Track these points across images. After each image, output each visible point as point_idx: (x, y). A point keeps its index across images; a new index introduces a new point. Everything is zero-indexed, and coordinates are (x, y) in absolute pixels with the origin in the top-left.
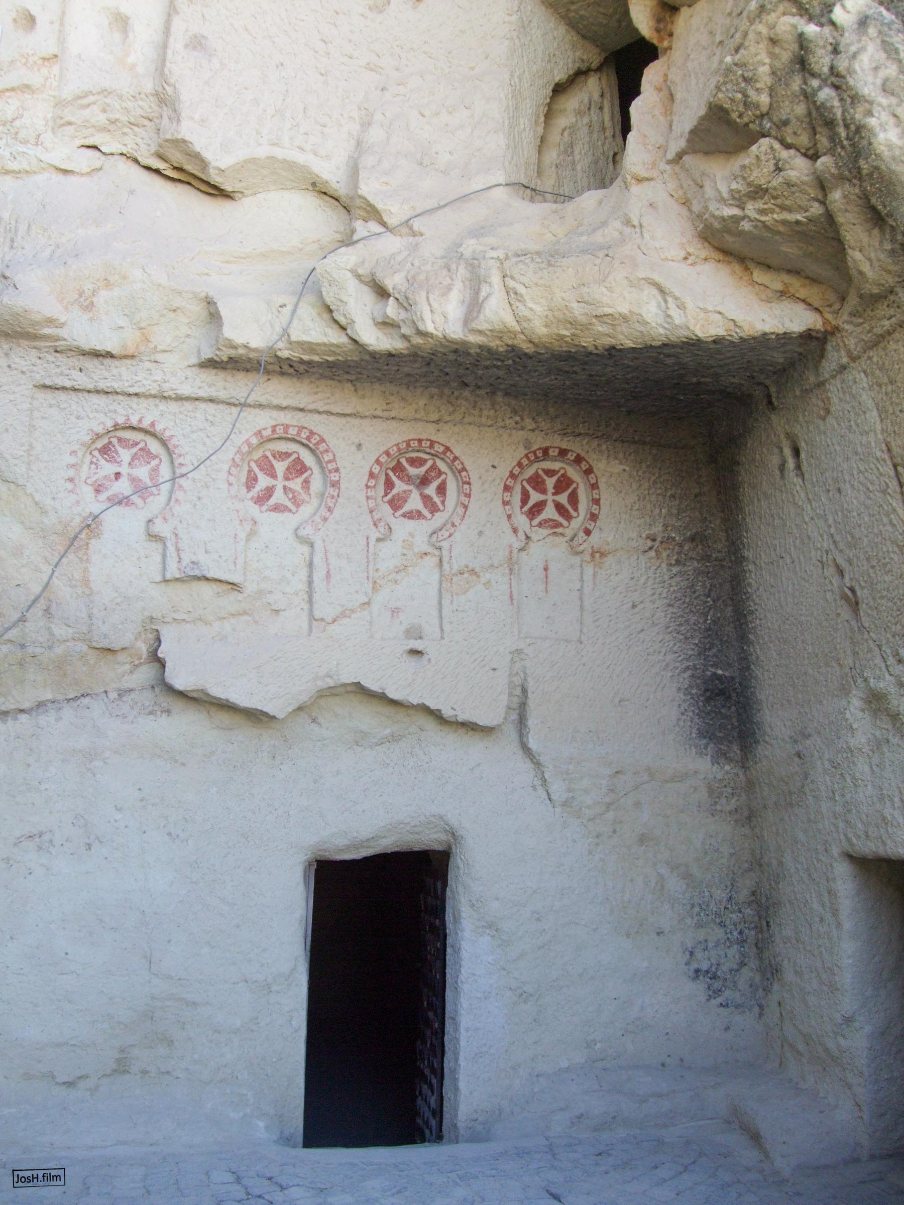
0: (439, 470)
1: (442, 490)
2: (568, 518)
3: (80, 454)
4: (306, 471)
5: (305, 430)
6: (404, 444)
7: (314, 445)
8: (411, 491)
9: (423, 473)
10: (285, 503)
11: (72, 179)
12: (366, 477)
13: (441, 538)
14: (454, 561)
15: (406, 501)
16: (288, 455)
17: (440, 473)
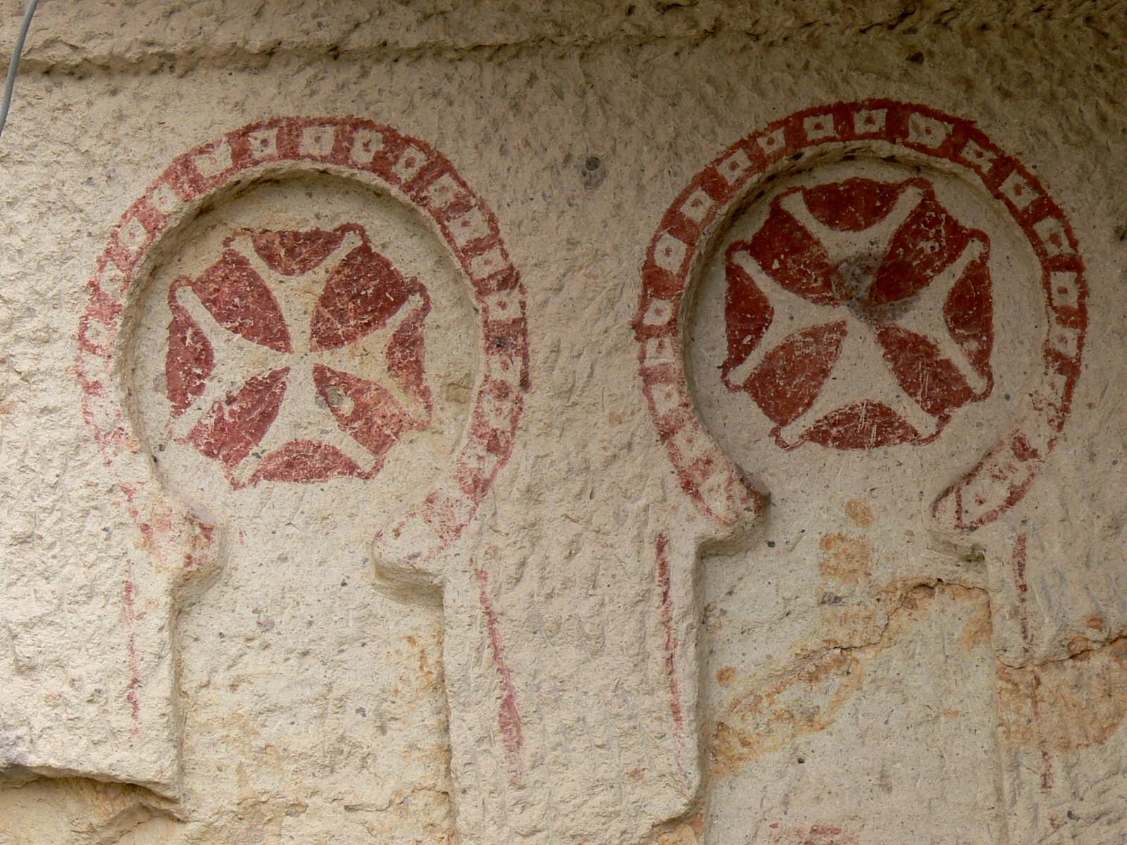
0: (953, 226)
4: (400, 300)
5: (362, 135)
6: (779, 136)
7: (408, 188)
8: (840, 328)
9: (883, 246)
10: (328, 440)
12: (632, 295)
13: (977, 512)
14: (1037, 602)
15: (825, 373)
16: (322, 242)
17: (958, 237)
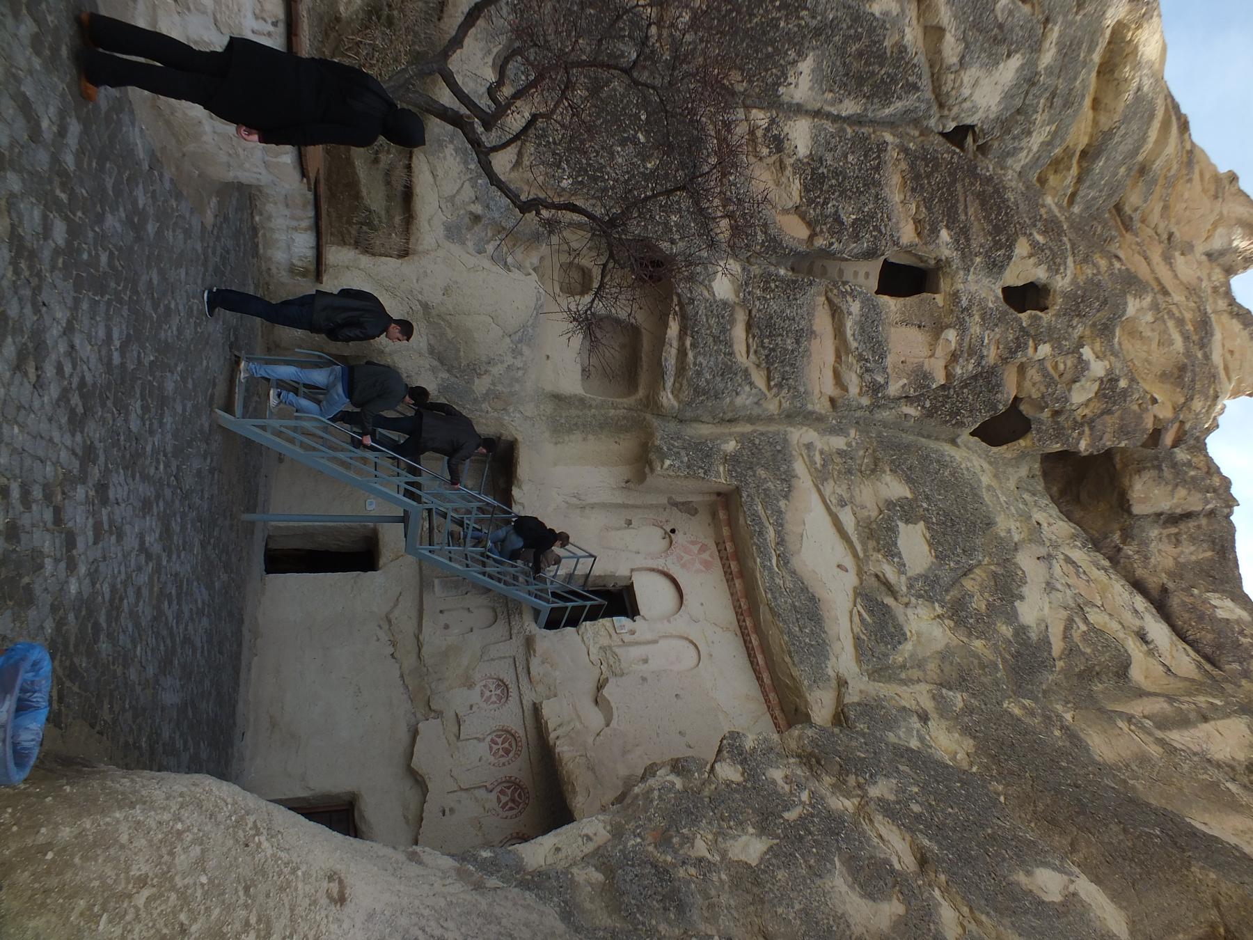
1: (511, 809)
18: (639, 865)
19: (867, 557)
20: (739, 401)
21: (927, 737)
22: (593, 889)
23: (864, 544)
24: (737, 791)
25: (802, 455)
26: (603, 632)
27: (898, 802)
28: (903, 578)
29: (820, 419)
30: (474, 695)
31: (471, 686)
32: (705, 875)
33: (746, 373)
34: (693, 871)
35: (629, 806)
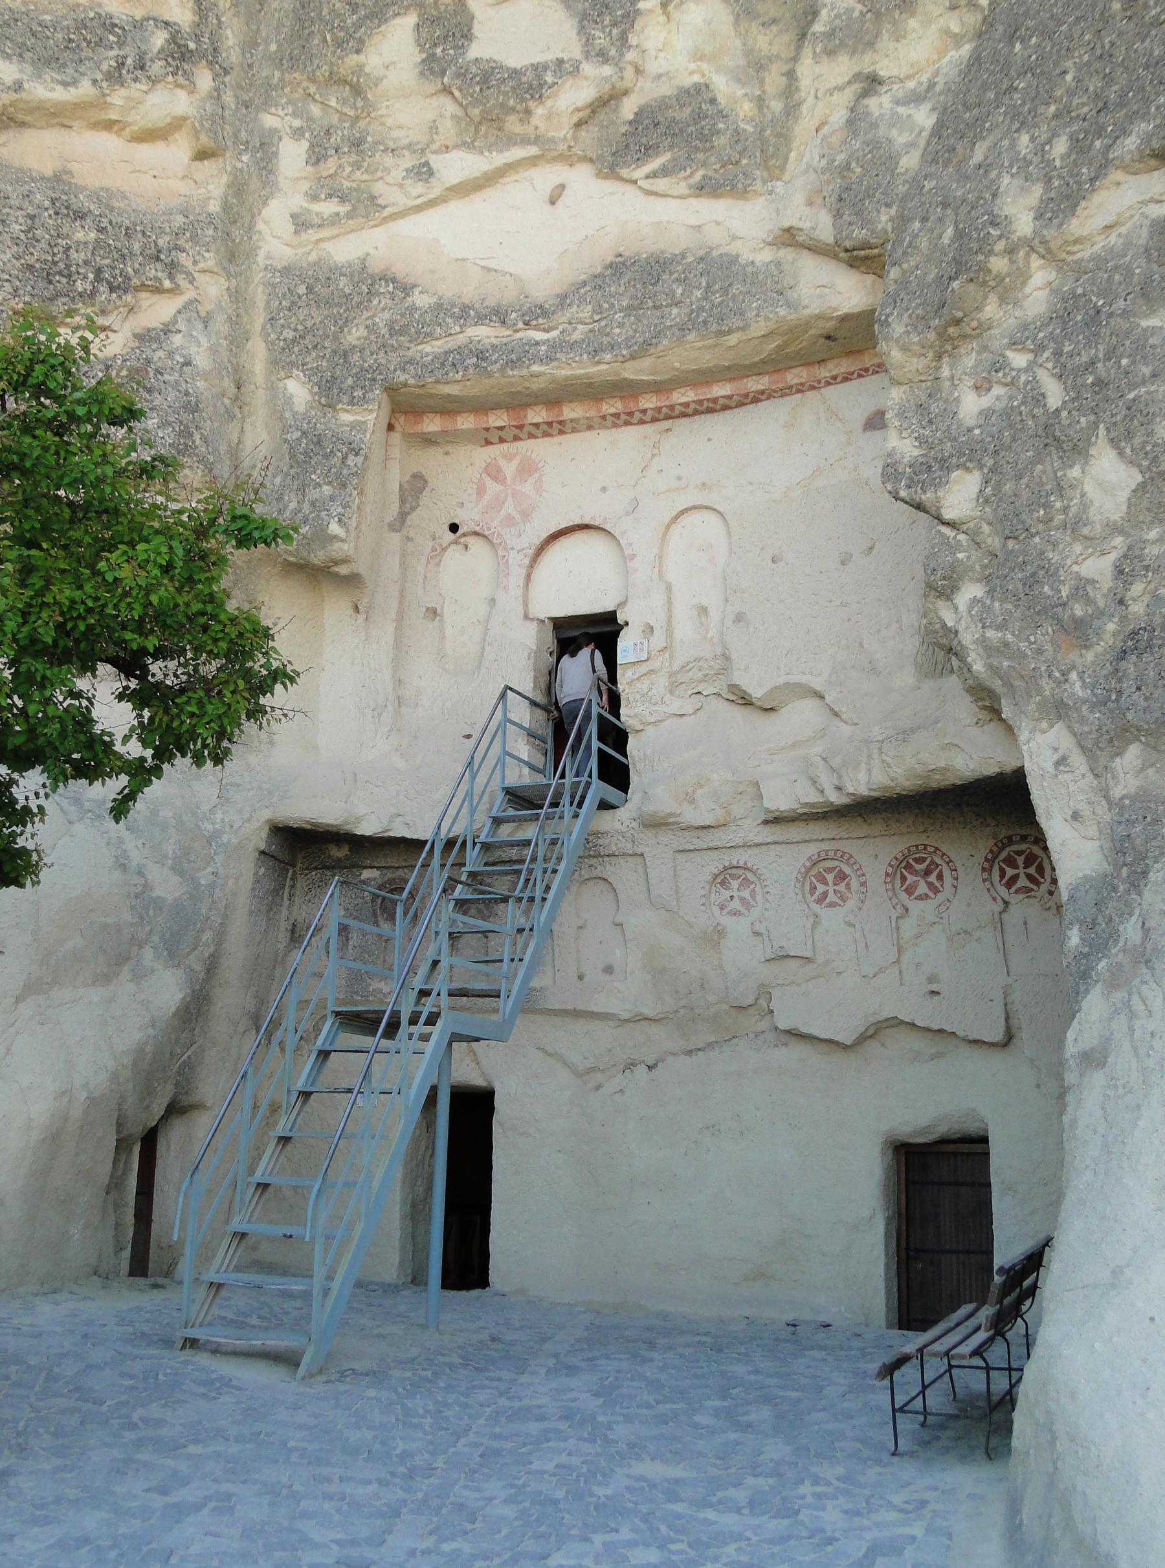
1: (940, 877)
2: (1038, 884)
3: (707, 888)
11: (685, 718)
16: (833, 869)
17: (937, 865)
18: (1120, 680)
19: (537, 140)
20: (202, 361)
21: (911, 84)
22: (1152, 765)
23: (513, 141)
24: (998, 486)
25: (318, 241)
26: (644, 686)
27: (1049, 181)
28: (588, 69)
29: (238, 187)
30: (737, 927)
31: (720, 932)
32: (1147, 568)
33: (144, 337)
34: (1137, 588)
35: (1008, 684)
